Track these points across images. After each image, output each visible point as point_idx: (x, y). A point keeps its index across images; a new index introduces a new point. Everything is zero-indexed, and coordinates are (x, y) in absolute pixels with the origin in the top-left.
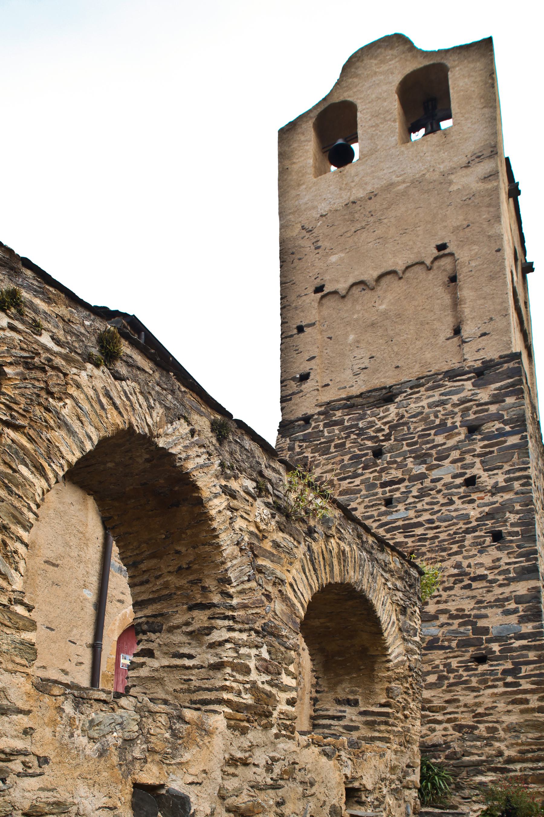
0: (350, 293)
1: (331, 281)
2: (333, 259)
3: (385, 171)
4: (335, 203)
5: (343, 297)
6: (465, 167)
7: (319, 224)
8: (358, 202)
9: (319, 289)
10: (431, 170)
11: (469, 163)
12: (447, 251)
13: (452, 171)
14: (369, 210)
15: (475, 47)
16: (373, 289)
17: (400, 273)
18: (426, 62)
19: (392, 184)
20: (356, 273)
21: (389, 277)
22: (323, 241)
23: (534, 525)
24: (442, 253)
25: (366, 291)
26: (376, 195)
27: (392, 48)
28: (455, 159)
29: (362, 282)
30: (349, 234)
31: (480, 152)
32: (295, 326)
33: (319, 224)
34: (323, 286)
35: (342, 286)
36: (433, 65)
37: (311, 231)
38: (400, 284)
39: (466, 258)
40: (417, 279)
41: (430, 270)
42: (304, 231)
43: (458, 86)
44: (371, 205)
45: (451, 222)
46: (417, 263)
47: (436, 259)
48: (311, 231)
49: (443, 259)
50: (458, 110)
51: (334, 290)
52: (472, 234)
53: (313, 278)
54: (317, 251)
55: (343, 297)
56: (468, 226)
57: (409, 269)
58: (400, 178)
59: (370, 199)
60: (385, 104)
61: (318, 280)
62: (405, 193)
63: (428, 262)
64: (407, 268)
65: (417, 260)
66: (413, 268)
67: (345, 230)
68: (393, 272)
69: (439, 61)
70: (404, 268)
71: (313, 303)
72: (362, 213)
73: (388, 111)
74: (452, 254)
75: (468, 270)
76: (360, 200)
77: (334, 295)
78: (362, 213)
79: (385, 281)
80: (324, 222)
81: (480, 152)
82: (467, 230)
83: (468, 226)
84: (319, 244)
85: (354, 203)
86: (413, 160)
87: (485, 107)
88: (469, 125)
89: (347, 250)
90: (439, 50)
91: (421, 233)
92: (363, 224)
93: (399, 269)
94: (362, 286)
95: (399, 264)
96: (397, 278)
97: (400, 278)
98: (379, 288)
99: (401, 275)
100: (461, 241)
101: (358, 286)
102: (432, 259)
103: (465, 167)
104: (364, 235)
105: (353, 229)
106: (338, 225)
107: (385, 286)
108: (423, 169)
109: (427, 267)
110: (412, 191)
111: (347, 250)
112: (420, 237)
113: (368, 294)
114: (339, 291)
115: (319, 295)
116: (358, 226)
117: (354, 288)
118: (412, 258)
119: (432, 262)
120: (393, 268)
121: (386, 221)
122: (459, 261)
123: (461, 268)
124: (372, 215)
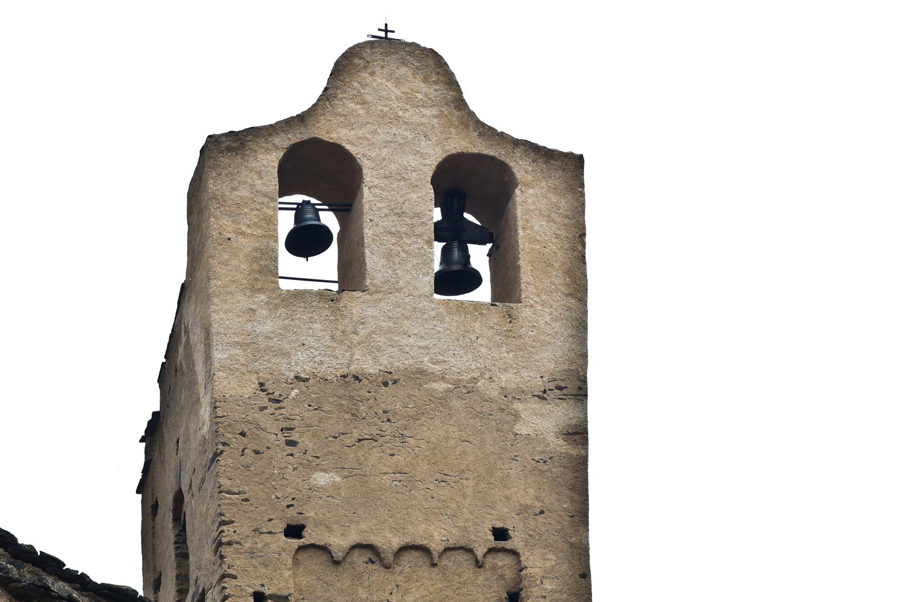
0: (349, 560)
1: (318, 523)
2: (322, 479)
3: (411, 340)
4: (322, 363)
5: (337, 563)
6: (539, 397)
7: (294, 393)
8: (365, 381)
9: (294, 531)
10: (487, 376)
11: (545, 392)
12: (508, 544)
13: (519, 395)
14: (384, 406)
15: (559, 163)
16: (387, 567)
17: (435, 554)
18: (480, 147)
19: (422, 372)
20: (363, 526)
21: (415, 554)
22: (302, 434)
23: (177, 555)
24: (501, 544)
25: (375, 567)
26: (395, 382)
27: (426, 80)
28: (525, 373)
29: (371, 547)
30: (348, 442)
31: (563, 380)
32: (251, 590)
33: (294, 393)
34: (302, 527)
35: (338, 542)
36: (492, 159)
37: (278, 401)
38: (433, 575)
39: (536, 570)
40: (460, 576)
41: (480, 567)
42: (263, 394)
43: (532, 228)
44: (390, 399)
45: (516, 493)
46: (461, 548)
47: (491, 550)
48: (278, 401)
49: (500, 555)
50: (530, 279)
51: (322, 543)
52: (547, 531)
53: (284, 504)
54: (290, 449)
55: (337, 563)
56: (542, 512)
57: (448, 553)
58: (437, 367)
59: (386, 384)
60: (414, 196)
61: (292, 512)
62: (442, 400)
63: (480, 552)
64: (447, 549)
65: (463, 543)
66: (455, 553)
67: (340, 428)
68: (424, 550)
69: (503, 158)
70: (441, 548)
71: (283, 554)
72: (371, 408)
73: (418, 215)
74: (514, 553)
75: (539, 594)
76: (368, 376)
77: (320, 553)
78: (371, 408)
79: (409, 559)
80: (302, 393)
81: (563, 380)
82: (540, 519)
83: (542, 512)
84: (295, 436)
85: (356, 378)
86: (458, 340)
87: (570, 295)
88: (548, 318)
89: (346, 473)
90: (502, 133)
91: (469, 492)
92: (375, 432)
93: (436, 546)
94: (368, 555)
95: (436, 536)
96: (428, 562)
97: (434, 565)
98: (398, 569)
99: (436, 560)
100: (531, 536)
101: (363, 551)
102: (485, 550)
103: (539, 397)
104: (375, 454)
105: (356, 435)
106: (330, 412)
107: (407, 570)
108: (473, 367)
109: (477, 561)
110: (457, 403)
111: (346, 473)
112: (468, 501)
113: (378, 574)
114: (332, 549)
115: (295, 543)
116: (366, 431)
117: (356, 552)
118: (455, 537)
119: (485, 555)
120: (425, 542)
121: (412, 441)
122: (529, 571)
123: (530, 586)
124: (389, 420)
